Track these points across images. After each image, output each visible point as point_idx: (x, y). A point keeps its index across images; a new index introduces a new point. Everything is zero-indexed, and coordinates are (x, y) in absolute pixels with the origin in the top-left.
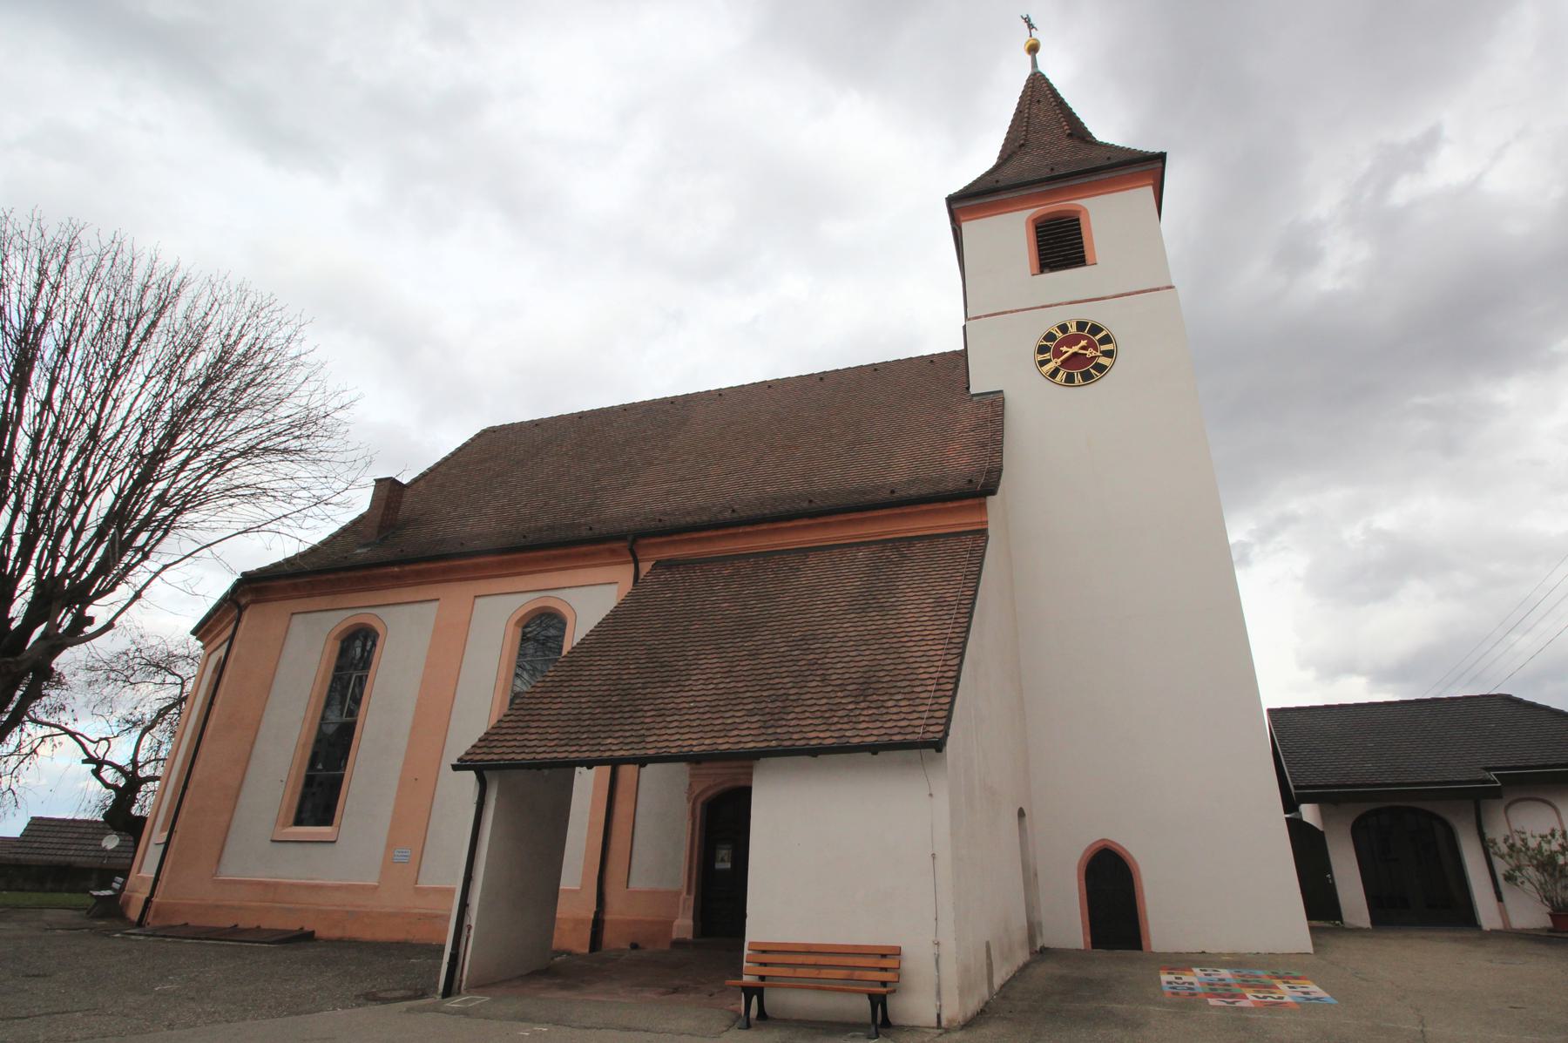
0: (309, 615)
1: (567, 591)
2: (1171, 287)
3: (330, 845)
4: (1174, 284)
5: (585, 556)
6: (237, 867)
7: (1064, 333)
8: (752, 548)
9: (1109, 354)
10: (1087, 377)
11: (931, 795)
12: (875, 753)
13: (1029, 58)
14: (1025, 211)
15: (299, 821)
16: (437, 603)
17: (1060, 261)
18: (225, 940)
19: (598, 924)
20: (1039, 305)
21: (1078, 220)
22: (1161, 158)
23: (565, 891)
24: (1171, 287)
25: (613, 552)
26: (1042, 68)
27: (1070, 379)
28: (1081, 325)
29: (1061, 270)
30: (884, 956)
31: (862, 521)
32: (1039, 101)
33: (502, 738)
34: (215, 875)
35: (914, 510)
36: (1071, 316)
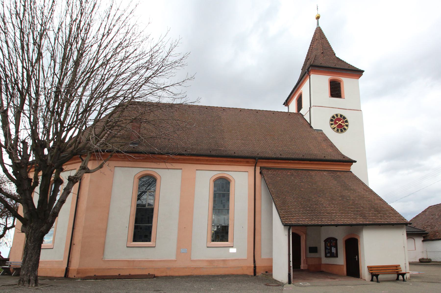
0: (123, 168)
1: (230, 172)
2: (361, 111)
3: (153, 248)
4: (361, 110)
5: (238, 162)
6: (110, 255)
7: (340, 117)
8: (289, 167)
11: (403, 234)
12: (380, 225)
13: (316, 21)
14: (328, 76)
15: (135, 240)
16: (181, 170)
17: (335, 95)
18: (133, 279)
19: (67, 270)
21: (340, 83)
22: (363, 71)
23: (41, 261)
25: (248, 162)
26: (320, 25)
27: (338, 130)
28: (341, 116)
31: (321, 164)
32: (323, 38)
34: (102, 259)
35: (336, 163)
36: (340, 112)
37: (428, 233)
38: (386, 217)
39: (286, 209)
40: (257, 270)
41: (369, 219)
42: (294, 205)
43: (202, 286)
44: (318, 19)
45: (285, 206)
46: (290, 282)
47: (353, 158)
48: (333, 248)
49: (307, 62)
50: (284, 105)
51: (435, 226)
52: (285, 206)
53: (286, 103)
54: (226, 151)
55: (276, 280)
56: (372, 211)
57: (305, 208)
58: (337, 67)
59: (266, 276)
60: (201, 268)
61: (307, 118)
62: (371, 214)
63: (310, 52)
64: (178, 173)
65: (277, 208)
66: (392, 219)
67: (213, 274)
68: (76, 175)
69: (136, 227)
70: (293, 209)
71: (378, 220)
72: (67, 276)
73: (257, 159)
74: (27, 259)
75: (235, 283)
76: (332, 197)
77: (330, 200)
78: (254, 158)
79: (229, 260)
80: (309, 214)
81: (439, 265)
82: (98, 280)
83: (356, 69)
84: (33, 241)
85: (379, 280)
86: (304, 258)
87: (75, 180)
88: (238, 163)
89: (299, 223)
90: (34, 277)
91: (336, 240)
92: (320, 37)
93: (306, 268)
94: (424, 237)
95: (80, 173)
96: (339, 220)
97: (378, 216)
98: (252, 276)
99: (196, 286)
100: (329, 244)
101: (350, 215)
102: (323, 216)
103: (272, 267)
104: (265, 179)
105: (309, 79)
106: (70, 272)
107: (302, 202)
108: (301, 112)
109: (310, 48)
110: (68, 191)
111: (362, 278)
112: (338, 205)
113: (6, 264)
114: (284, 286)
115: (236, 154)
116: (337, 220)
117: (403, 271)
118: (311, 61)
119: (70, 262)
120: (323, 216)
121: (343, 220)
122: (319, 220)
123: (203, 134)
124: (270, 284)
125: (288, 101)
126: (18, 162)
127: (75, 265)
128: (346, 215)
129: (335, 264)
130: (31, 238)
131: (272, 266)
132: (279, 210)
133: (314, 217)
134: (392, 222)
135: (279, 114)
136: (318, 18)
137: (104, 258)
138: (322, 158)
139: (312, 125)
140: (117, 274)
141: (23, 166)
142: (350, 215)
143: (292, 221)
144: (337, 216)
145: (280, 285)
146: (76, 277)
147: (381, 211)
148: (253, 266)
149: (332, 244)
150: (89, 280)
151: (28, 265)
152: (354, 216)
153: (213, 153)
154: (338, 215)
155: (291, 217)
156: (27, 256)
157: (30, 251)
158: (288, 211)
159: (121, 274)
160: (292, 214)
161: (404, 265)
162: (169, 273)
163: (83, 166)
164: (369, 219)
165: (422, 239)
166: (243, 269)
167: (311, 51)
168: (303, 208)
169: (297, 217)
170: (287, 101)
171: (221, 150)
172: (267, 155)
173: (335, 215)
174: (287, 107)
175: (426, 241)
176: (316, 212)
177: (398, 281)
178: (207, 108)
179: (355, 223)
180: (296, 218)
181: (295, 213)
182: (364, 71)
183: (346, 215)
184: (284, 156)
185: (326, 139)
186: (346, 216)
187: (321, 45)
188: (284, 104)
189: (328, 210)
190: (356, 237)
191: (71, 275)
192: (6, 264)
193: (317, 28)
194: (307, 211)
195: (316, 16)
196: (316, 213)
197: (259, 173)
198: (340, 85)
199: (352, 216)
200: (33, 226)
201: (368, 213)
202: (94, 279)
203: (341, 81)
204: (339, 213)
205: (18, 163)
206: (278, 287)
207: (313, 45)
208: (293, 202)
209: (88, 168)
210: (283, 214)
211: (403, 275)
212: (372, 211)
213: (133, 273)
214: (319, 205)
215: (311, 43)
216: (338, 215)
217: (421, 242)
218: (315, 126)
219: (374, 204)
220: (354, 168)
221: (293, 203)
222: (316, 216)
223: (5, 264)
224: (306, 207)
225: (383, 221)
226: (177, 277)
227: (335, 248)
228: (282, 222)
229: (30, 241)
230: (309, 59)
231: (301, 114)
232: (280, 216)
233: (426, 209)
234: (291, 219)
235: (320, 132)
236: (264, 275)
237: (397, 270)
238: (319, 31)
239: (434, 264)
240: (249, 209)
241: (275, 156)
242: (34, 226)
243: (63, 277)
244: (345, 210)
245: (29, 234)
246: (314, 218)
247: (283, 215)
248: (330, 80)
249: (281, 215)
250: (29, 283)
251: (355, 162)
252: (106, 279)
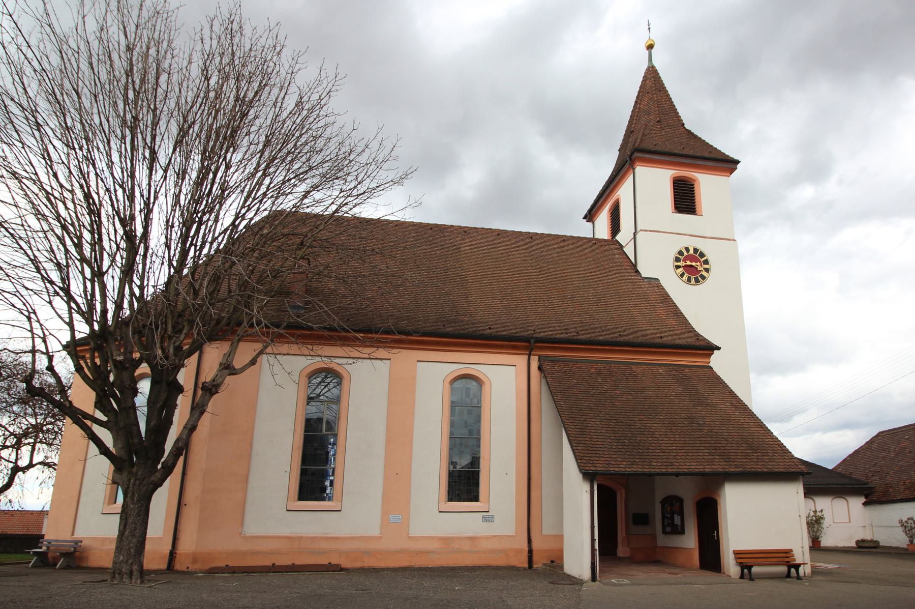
2: (734, 240)
9: (707, 270)
10: (697, 281)
13: (647, 52)
15: (302, 497)
19: (172, 555)
20: (675, 232)
21: (693, 185)
22: (737, 162)
24: (734, 240)
25: (515, 348)
28: (696, 250)
29: (685, 213)
30: (786, 553)
33: (657, 458)
36: (693, 243)
37: (874, 487)
38: (767, 461)
39: (588, 442)
40: (535, 557)
41: (735, 463)
42: (601, 434)
43: (437, 584)
44: (650, 49)
45: (585, 436)
46: (594, 578)
47: (715, 341)
48: (675, 516)
49: (629, 137)
50: (585, 220)
51: (888, 473)
52: (585, 436)
53: (590, 216)
54: (473, 324)
55: (569, 576)
56: (742, 448)
57: (621, 441)
58: (687, 153)
59: (552, 569)
60: (428, 552)
61: (629, 251)
62: (740, 454)
63: (635, 118)
64: (383, 367)
65: (570, 441)
66: (777, 464)
67: (451, 564)
68: (214, 381)
69: (303, 472)
70: (600, 443)
71: (752, 466)
72: (171, 568)
73: (532, 341)
74: (127, 533)
75: (494, 579)
76: (671, 420)
77: (667, 425)
78: (527, 340)
79: (479, 538)
80: (628, 453)
81: (891, 553)
82: (236, 575)
83: (723, 158)
84: (138, 500)
85: (753, 577)
86: (624, 535)
87: (213, 390)
88: (498, 349)
89: (609, 468)
90: (138, 566)
91: (681, 501)
92: (654, 88)
93: (628, 555)
94: (866, 497)
95: (221, 377)
96: (682, 464)
97: (753, 457)
98: (525, 569)
99: (427, 583)
100: (669, 509)
101: (701, 454)
102: (653, 457)
103: (561, 551)
104: (547, 383)
105: (632, 175)
106: (177, 560)
107: (617, 430)
108: (618, 238)
109: (635, 106)
110: (201, 409)
111: (724, 573)
112: (682, 436)
113: (40, 545)
114: (584, 584)
115: (493, 332)
116: (678, 464)
117: (798, 561)
118: (638, 136)
119: (178, 539)
120: (653, 457)
121: (689, 464)
122: (645, 463)
123: (427, 285)
124: (559, 582)
125: (592, 213)
126: (120, 359)
127: (186, 545)
128: (695, 454)
129: (684, 547)
130: (133, 494)
131: (563, 550)
132: (574, 445)
133: (637, 459)
134: (776, 470)
136: (650, 47)
137: (243, 533)
138: (657, 340)
139: (640, 268)
140: (268, 563)
141: (128, 365)
142: (701, 454)
143: (597, 465)
144: (679, 458)
145: (577, 584)
146: (190, 569)
147: (760, 448)
148: (527, 549)
149: (674, 509)
150: (221, 575)
151: (129, 544)
152: (709, 457)
153: (449, 329)
154: (681, 454)
155: (596, 459)
156: (127, 527)
157: (132, 518)
158: (591, 445)
159: (277, 564)
160: (598, 452)
161: (801, 549)
162: (369, 563)
163: (225, 364)
164: (735, 463)
165: (863, 500)
166: (507, 555)
167: (637, 116)
168: (618, 441)
169: (607, 459)
170: (590, 211)
171: (462, 321)
172: (551, 335)
173: (675, 454)
174: (590, 224)
175: (870, 504)
176: (642, 448)
177: (788, 579)
178: (431, 229)
179: (710, 470)
180: (604, 459)
181: (603, 449)
183: (695, 454)
184: (584, 337)
185: (665, 298)
186: (694, 457)
187: (656, 105)
188: (584, 218)
189: (663, 445)
191: (178, 566)
192: (40, 545)
193: (648, 69)
194: (626, 447)
195: (647, 43)
196: (640, 451)
197: (537, 369)
198: (693, 188)
199: (706, 458)
200: (136, 473)
201: (735, 451)
202: (229, 573)
203: (695, 180)
204: (683, 451)
205: (120, 362)
206: (572, 586)
207: (640, 104)
208: (600, 429)
209: (233, 366)
210: (582, 451)
211: (797, 567)
212: (742, 448)
213: (298, 562)
214: (646, 436)
215: (638, 97)
216: (681, 454)
217: (861, 504)
218: (645, 270)
219: (747, 434)
220: (716, 362)
221: (599, 431)
222: (640, 457)
223: (38, 544)
224: (622, 438)
225: (759, 468)
226: (383, 569)
227: (679, 517)
228: (579, 466)
229: (133, 499)
230: (632, 132)
231: (617, 241)
232: (575, 457)
233: (873, 437)
234: (595, 462)
235: (654, 283)
236: (548, 568)
237: (787, 560)
238: (652, 75)
239: (881, 553)
240: (517, 438)
241: (567, 334)
242: (139, 473)
243: (164, 570)
244: (694, 445)
245: (128, 487)
246: (637, 461)
247: (581, 455)
248: (674, 178)
249: (578, 454)
250: (131, 578)
251: (718, 348)
252: (252, 573)
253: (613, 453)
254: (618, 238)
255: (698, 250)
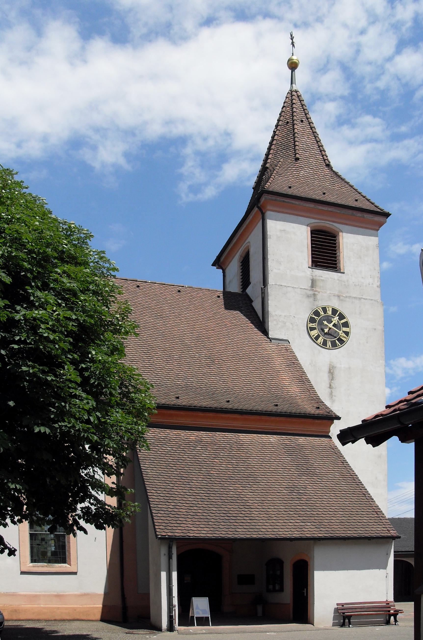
11: (387, 554)
22: (387, 215)
28: (334, 311)
79: (69, 595)
135: (194, 294)
138: (271, 408)
155: (176, 525)
182: (390, 214)
188: (213, 265)
190: (307, 560)
237: (388, 609)
251: (338, 418)
253: (197, 520)
254: (249, 291)
255: (338, 311)
